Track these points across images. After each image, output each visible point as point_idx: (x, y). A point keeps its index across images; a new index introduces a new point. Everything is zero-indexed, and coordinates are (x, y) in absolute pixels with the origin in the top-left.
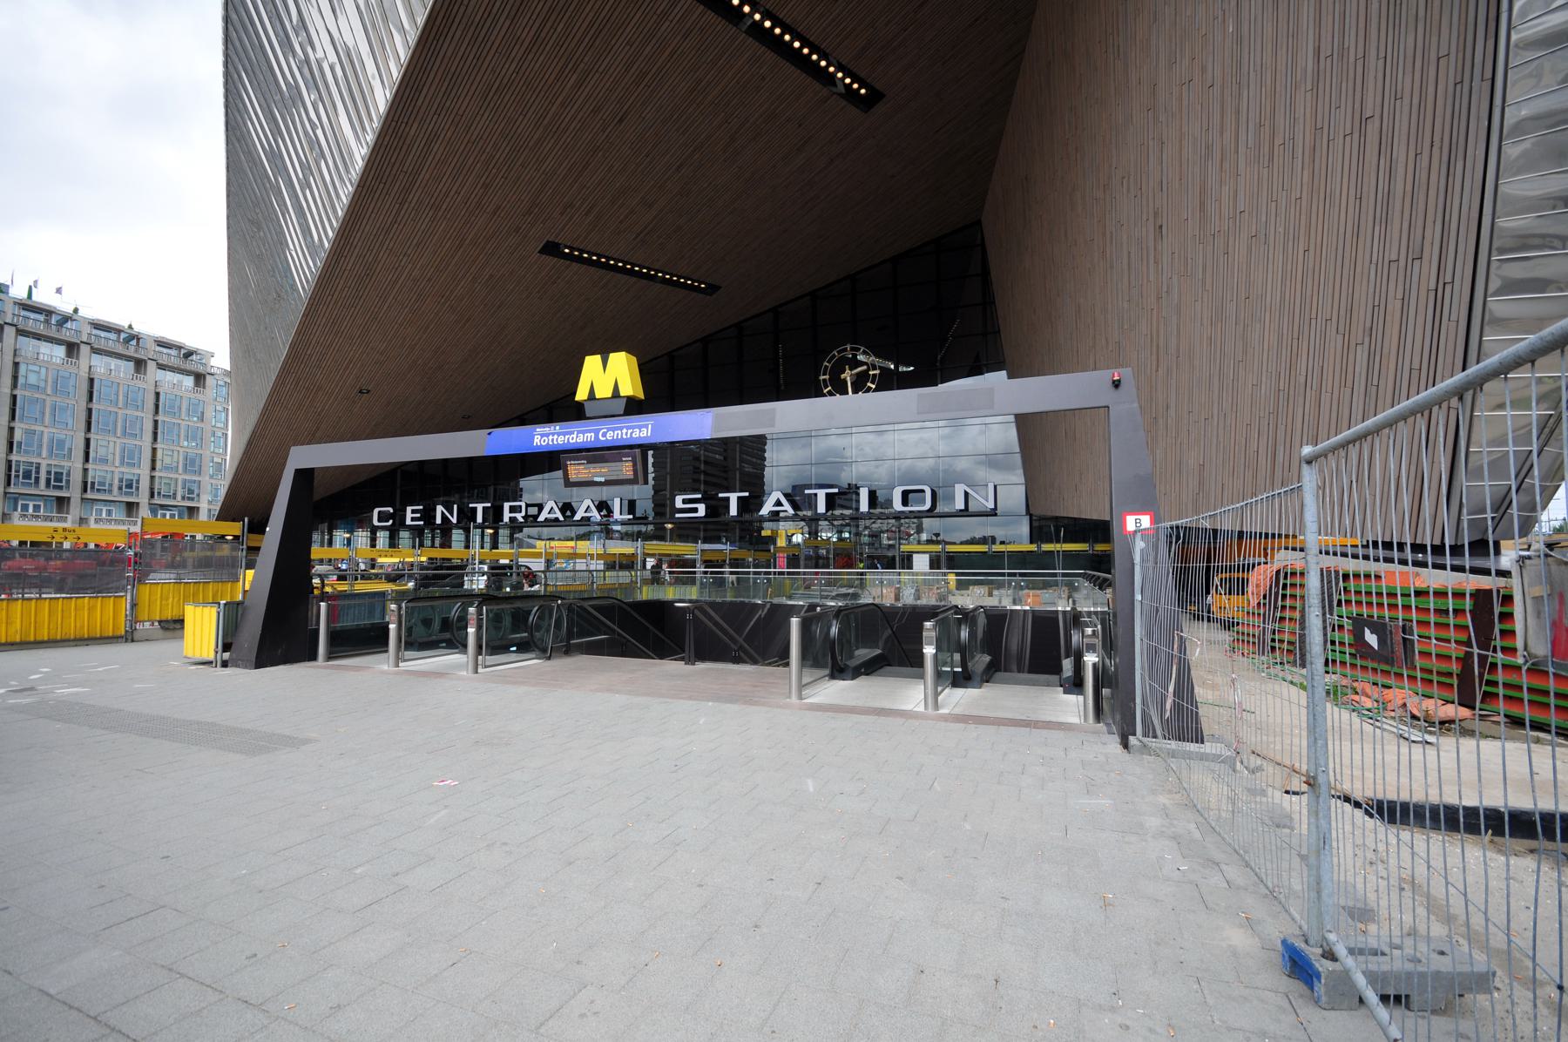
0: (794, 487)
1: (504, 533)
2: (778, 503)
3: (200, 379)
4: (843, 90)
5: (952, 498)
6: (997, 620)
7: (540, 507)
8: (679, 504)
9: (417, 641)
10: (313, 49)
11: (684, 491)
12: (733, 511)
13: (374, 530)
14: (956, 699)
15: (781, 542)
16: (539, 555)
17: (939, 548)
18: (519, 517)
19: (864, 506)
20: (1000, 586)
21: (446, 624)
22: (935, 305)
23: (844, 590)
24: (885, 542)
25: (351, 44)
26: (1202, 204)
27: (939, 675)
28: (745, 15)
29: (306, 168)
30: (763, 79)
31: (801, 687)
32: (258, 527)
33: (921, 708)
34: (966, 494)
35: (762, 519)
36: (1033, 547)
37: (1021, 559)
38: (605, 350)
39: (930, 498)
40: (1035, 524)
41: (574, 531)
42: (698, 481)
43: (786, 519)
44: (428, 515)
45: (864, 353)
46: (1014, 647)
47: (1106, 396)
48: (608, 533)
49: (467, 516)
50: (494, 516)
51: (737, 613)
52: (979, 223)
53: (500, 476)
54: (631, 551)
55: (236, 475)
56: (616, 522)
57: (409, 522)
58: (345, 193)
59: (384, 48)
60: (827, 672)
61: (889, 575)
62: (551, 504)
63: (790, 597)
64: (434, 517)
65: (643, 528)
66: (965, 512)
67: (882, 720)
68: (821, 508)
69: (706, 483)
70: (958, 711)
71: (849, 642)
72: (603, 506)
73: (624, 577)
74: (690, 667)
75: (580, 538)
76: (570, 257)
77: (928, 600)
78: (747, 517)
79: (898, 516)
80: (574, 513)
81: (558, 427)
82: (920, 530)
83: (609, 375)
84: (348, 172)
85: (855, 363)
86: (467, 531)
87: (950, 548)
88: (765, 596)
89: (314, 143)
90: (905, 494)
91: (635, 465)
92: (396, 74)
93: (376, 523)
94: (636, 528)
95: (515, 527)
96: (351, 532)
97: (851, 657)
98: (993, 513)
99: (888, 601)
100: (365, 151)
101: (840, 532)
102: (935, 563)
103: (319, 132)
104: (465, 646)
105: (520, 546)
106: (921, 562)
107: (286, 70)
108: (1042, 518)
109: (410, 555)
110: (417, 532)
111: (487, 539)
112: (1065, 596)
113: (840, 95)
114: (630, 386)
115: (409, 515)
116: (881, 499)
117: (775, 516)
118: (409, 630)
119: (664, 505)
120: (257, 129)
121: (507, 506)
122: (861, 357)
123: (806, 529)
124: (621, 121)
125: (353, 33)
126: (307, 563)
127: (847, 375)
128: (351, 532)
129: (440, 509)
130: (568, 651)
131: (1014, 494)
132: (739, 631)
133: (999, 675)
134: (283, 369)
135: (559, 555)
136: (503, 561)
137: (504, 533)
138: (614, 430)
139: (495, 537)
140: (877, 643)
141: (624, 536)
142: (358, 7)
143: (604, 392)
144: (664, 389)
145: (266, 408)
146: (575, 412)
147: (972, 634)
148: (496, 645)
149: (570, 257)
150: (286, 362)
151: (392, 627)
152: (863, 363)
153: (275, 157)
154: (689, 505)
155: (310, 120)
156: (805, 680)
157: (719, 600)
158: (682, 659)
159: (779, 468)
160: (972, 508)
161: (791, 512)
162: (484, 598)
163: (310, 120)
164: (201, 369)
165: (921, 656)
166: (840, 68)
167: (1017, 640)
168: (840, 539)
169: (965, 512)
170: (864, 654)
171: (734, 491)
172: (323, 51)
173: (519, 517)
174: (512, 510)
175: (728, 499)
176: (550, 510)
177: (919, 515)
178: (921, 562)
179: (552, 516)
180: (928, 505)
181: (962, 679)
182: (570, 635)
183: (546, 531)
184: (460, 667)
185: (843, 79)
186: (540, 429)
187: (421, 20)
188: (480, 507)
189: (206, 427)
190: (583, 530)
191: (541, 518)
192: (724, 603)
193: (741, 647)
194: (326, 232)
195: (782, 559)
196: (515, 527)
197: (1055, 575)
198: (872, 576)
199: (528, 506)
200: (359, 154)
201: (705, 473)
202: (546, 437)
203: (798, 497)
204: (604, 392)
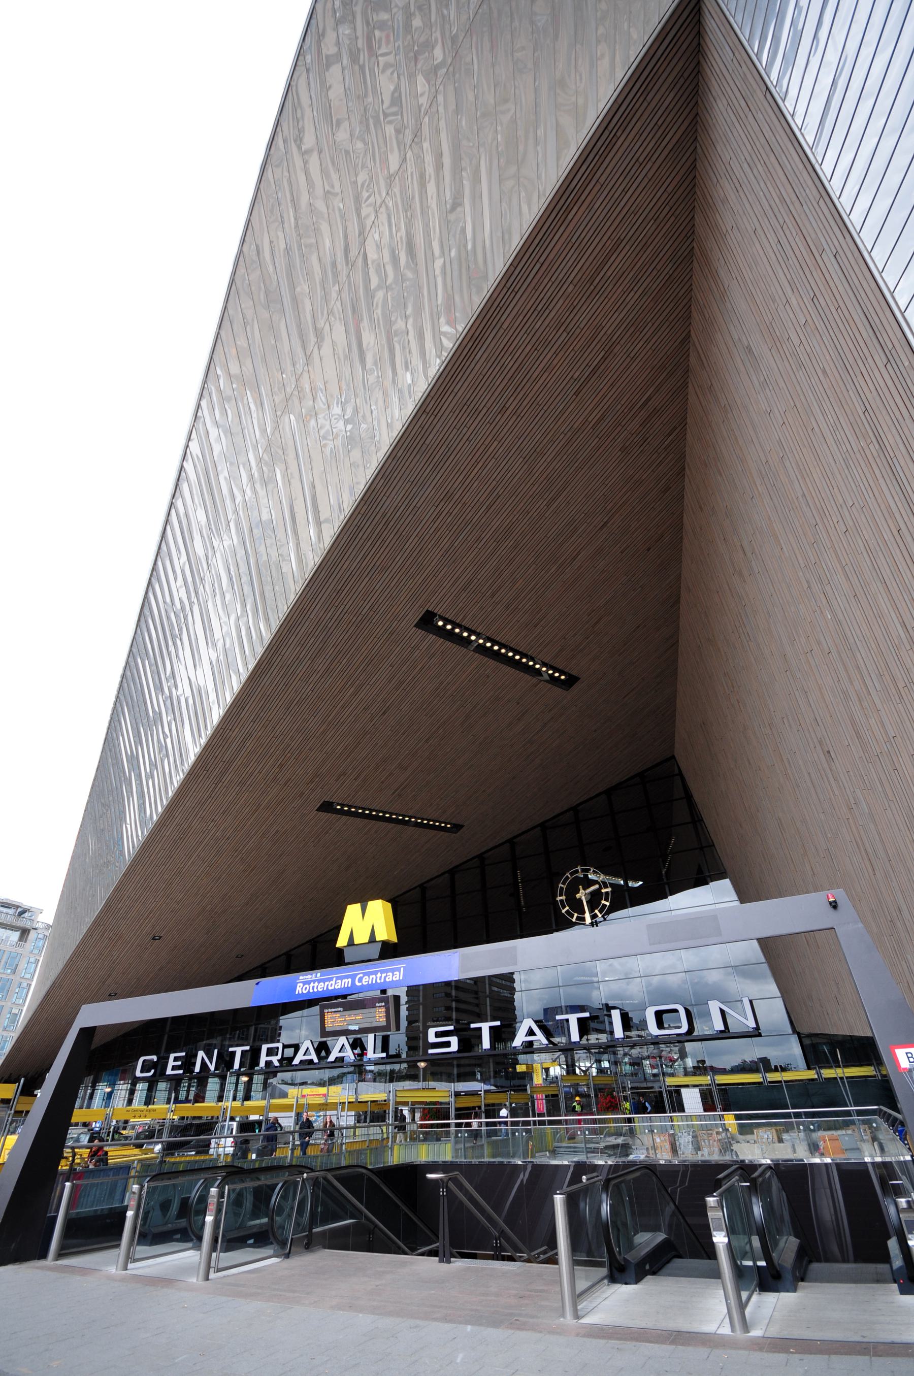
0: (546, 1010)
1: (258, 1079)
2: (531, 1032)
3: (24, 933)
4: (548, 678)
5: (707, 1015)
6: (793, 1176)
7: (297, 1047)
8: (432, 1039)
9: (153, 1235)
10: (176, 689)
11: (437, 1021)
12: (486, 1044)
13: (135, 1081)
14: (770, 1309)
15: (538, 1079)
16: (288, 1108)
17: (706, 1080)
18: (275, 1060)
19: (619, 1033)
20: (788, 1128)
21: (185, 1208)
22: (650, 827)
23: (613, 1141)
24: (649, 1071)
25: (202, 684)
26: (859, 736)
27: (740, 1273)
28: (472, 641)
29: (153, 765)
30: (488, 677)
31: (577, 1297)
32: (28, 1091)
33: (726, 1330)
34: (723, 1012)
35: (516, 1052)
36: (812, 1074)
37: (805, 1094)
38: (363, 900)
39: (685, 1020)
40: (807, 1042)
41: (326, 1074)
42: (448, 1008)
43: (541, 1050)
44: (187, 1064)
45: (594, 872)
46: (827, 1214)
47: (828, 919)
48: (359, 1070)
49: (226, 1061)
50: (252, 1057)
51: (492, 1179)
52: (673, 757)
53: (260, 1022)
54: (381, 1097)
55: (26, 1027)
56: (370, 1062)
57: (169, 1071)
58: (177, 779)
59: (224, 685)
60: (604, 1271)
61: (658, 1120)
62: (306, 1044)
63: (554, 1153)
64: (194, 1064)
65: (396, 1067)
66: (725, 1034)
67: (682, 1351)
68: (575, 1036)
69: (457, 1010)
70: (774, 1332)
71: (625, 1225)
72: (357, 1044)
73: (375, 1132)
74: (445, 1266)
75: (332, 1081)
76: (341, 812)
77: (710, 1154)
78: (501, 1046)
79: (656, 1042)
80: (328, 1053)
81: (318, 974)
82: (683, 1055)
83: (368, 922)
84: (182, 764)
85: (588, 883)
86: (223, 1078)
87: (722, 1079)
88: (525, 1155)
89: (163, 748)
90: (659, 1015)
91: (387, 1012)
92: (229, 699)
93: (138, 1074)
94: (388, 1068)
95: (270, 1071)
96: (112, 1084)
97: (631, 1246)
98: (756, 1033)
99: (663, 1157)
100: (198, 750)
101: (599, 1061)
102: (708, 1104)
103: (169, 741)
104: (200, 1239)
105: (272, 1096)
106: (692, 1099)
107: (155, 702)
108: (810, 1036)
109: (165, 1110)
110: (176, 1082)
111: (241, 1087)
112: (867, 1137)
113: (546, 681)
114: (386, 932)
115: (171, 1063)
116: (636, 1021)
117: (529, 1047)
118: (146, 1214)
119: (416, 1038)
120: (125, 743)
121: (265, 1048)
122: (591, 876)
123: (563, 1058)
124: (384, 713)
125: (204, 678)
126: (67, 1123)
127: (582, 895)
128: (112, 1084)
129: (201, 1054)
130: (310, 1244)
131: (773, 1012)
132: (497, 1208)
133: (816, 1267)
134: (95, 922)
135: (310, 1107)
136: (254, 1117)
137: (258, 1079)
138: (369, 974)
139: (249, 1084)
140: (652, 1226)
141: (378, 1077)
142: (211, 663)
143: (361, 938)
144: (412, 938)
145: (71, 959)
146: (337, 959)
147: (769, 1209)
148: (234, 1239)
149: (341, 812)
150: (98, 917)
151: (130, 1214)
152: (595, 882)
153: (133, 759)
154: (441, 1039)
155: (163, 732)
156: (582, 1285)
157: (475, 1161)
158: (433, 1253)
159: (528, 1003)
160: (733, 1029)
161: (545, 1041)
162: (233, 1171)
163: (163, 732)
164: (28, 925)
165: (712, 1245)
166: (544, 664)
167: (829, 1206)
168: (601, 1071)
169: (725, 1034)
170: (646, 1241)
171: (487, 1021)
172: (184, 690)
173: (275, 1060)
174: (270, 1052)
175: (480, 1029)
176: (307, 1052)
177: (680, 1040)
178: (692, 1099)
179: (307, 1058)
180: (685, 1028)
181: (770, 1280)
182: (313, 1222)
183: (299, 1076)
184: (187, 1270)
185: (547, 672)
186: (303, 977)
187: (251, 667)
188: (238, 1050)
189: (16, 978)
190: (336, 1072)
191: (296, 1061)
192: (481, 1165)
193: (502, 1232)
194: (155, 809)
195: (541, 1105)
196: (270, 1071)
197: (848, 1113)
198: (641, 1121)
199: (285, 1047)
200: (193, 751)
201: (458, 1001)
202: (308, 983)
203: (549, 1024)
204: (361, 938)
